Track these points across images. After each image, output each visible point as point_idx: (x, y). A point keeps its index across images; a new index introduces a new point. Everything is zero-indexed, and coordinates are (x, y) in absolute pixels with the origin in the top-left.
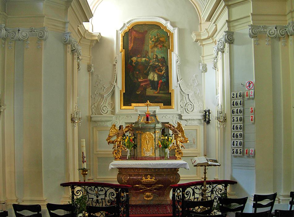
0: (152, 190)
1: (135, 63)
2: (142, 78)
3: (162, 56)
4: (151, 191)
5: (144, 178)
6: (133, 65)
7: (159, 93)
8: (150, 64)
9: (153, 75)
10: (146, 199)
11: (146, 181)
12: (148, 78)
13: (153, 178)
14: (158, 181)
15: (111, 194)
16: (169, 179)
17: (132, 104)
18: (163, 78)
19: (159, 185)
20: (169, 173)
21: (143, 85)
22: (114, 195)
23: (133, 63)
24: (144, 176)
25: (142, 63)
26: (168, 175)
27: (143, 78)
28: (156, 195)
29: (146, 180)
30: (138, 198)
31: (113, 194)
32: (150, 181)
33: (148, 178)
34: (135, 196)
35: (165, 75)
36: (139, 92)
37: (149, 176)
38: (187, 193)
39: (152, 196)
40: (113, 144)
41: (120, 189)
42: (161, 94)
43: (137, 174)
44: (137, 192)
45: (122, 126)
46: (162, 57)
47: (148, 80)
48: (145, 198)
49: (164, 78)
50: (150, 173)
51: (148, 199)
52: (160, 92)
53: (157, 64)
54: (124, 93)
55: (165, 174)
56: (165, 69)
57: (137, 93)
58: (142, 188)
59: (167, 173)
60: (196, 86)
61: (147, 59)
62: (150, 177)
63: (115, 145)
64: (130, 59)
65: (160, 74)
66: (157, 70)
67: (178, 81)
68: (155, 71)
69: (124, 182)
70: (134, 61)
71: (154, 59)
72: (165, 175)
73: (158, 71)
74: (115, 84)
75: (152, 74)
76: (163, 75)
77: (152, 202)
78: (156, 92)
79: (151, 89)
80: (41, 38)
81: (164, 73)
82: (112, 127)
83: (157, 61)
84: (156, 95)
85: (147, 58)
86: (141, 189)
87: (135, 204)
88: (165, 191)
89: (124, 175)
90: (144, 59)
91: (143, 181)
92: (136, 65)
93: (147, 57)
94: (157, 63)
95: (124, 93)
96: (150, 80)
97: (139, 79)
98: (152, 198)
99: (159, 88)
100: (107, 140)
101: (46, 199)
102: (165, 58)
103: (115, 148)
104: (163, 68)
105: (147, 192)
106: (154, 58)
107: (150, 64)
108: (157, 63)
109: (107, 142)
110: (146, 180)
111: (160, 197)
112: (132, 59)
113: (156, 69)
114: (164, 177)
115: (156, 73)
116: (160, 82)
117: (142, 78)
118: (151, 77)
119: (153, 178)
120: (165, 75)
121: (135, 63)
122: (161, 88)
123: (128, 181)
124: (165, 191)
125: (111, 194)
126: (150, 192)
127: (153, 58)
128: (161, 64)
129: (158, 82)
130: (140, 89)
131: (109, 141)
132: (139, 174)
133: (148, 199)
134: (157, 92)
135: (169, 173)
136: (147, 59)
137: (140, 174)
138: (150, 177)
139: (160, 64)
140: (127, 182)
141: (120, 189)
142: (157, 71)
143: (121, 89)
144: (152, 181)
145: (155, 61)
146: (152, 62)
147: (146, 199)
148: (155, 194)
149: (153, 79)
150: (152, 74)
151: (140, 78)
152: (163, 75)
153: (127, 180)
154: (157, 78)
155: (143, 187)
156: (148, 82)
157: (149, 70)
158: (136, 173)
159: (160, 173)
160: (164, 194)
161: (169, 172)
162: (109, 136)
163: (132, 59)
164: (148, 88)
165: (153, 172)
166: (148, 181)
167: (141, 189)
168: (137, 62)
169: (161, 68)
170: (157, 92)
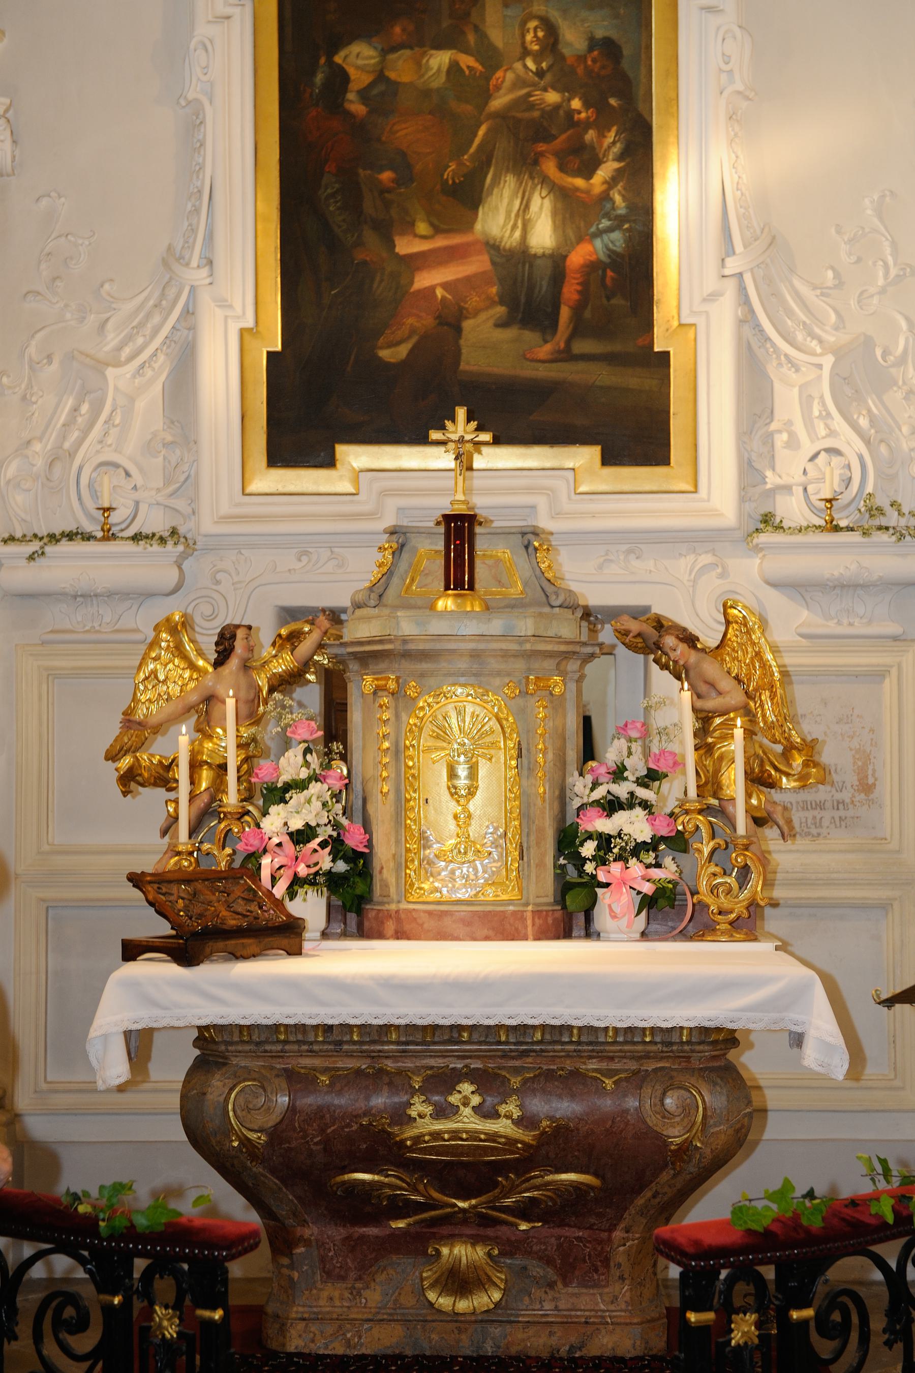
0: (496, 1222)
1: (364, 95)
2: (422, 227)
3: (600, 34)
4: (490, 1232)
5: (419, 1107)
6: (349, 114)
7: (566, 355)
8: (498, 102)
9: (517, 203)
10: (445, 1302)
11: (436, 1135)
12: (478, 226)
13: (503, 1109)
14: (544, 1139)
15: (59, 1310)
16: (653, 1121)
17: (342, 450)
18: (605, 223)
19: (564, 1176)
20: (651, 1066)
21: (432, 289)
22: (81, 1325)
23: (351, 96)
24: (422, 1091)
25: (427, 93)
26: (637, 1080)
27: (432, 225)
28: (537, 1269)
29: (439, 1126)
30: (374, 1296)
31: (69, 1312)
32: (473, 1135)
33: (455, 1110)
34: (343, 1278)
35: (618, 198)
36: (403, 351)
37: (467, 1088)
38: (836, 1316)
39: (499, 1277)
40: (161, 793)
41: (140, 1264)
42: (581, 365)
43: (359, 1072)
44: (362, 1237)
45: (240, 634)
46: (593, 43)
47: (477, 242)
48: (432, 1296)
49: (610, 230)
50: (476, 1064)
51: (463, 1305)
52: (582, 346)
53: (557, 107)
54: (270, 354)
55: (610, 1073)
56: (617, 149)
57: (385, 354)
58: (407, 1202)
59: (633, 1066)
60: (883, 291)
61: (467, 61)
62: (476, 1100)
63: (176, 801)
64: (323, 60)
65: (577, 189)
66: (556, 154)
67: (730, 250)
68: (536, 162)
69: (245, 1142)
70: (359, 79)
71: (530, 64)
72: (609, 1083)
73: (562, 168)
74: (199, 276)
75: (507, 193)
76: (605, 197)
77: (496, 1331)
78: (545, 350)
79: (502, 324)
80: (48, 288)
81: (611, 183)
82: (155, 643)
83: (548, 77)
84: (543, 372)
85: (467, 51)
86: (401, 1208)
87: (340, 1351)
88: (611, 1230)
89: (248, 1074)
90: (440, 60)
91: (418, 1139)
92: (370, 113)
93: (471, 38)
94: (552, 97)
95: (270, 354)
96: (492, 247)
97: (403, 233)
98: (497, 1296)
99: (565, 313)
100: (112, 756)
101: (607, 885)
102: (626, 52)
103: (176, 836)
104: (601, 135)
105: (451, 1239)
106: (526, 52)
107: (498, 102)
108: (552, 97)
109: (110, 772)
110: (439, 1126)
111: (566, 1285)
112: (338, 59)
113: (542, 147)
114: (607, 1104)
115: (545, 180)
116: (578, 257)
117: (422, 227)
118: (501, 219)
119: (503, 1109)
120: (618, 198)
121: (364, 95)
122: (587, 314)
123: (276, 1134)
124: (618, 1234)
125: (59, 1310)
126: (475, 1240)
127: (518, 50)
128: (587, 104)
129: (557, 260)
130: (410, 321)
131: (126, 762)
132: (381, 1071)
133: (463, 1305)
134: (548, 347)
135: (651, 1066)
136: (467, 61)
137: (390, 1065)
138: (476, 1100)
139: (576, 104)
140: (270, 1143)
141: (140, 1264)
142: (550, 167)
143: (249, 322)
144: (492, 1137)
145: (540, 74)
146: (515, 86)
147: (445, 1302)
148: (529, 1253)
149: (518, 234)
150: (507, 193)
151: (412, 224)
152: (605, 197)
153: (272, 1120)
154: (555, 228)
155: (416, 1191)
156: (478, 264)
157: (485, 161)
158: (351, 1064)
159: (569, 1065)
160: (606, 1262)
161: (647, 1056)
162: (129, 721)
163: (338, 59)
164: (476, 313)
165: (505, 1055)
166: (455, 1134)
167: (401, 1208)
168: (381, 88)
169: (590, 135)
170: (548, 347)
